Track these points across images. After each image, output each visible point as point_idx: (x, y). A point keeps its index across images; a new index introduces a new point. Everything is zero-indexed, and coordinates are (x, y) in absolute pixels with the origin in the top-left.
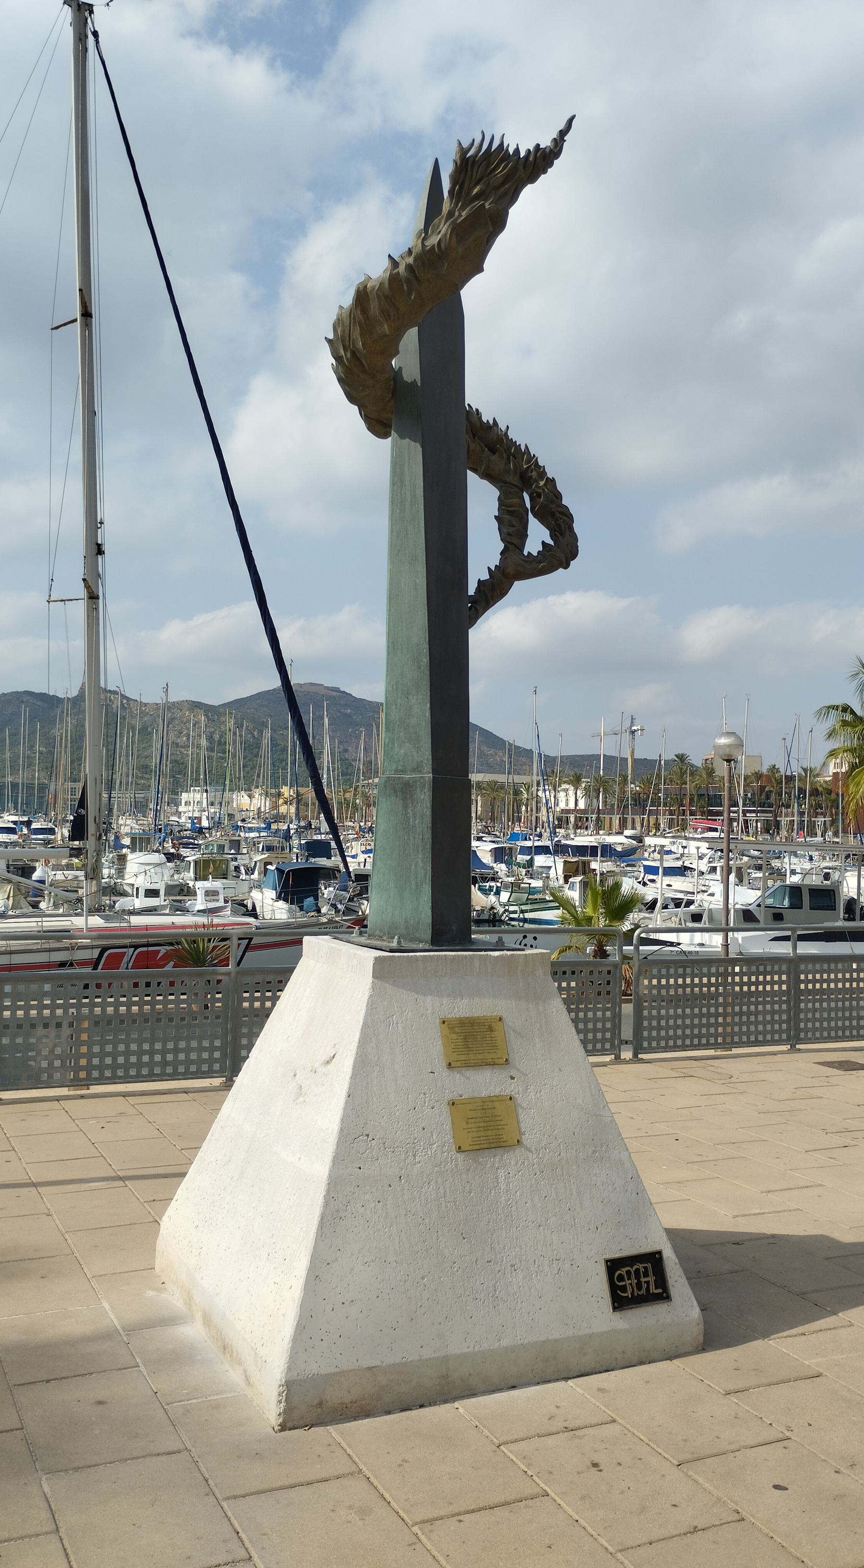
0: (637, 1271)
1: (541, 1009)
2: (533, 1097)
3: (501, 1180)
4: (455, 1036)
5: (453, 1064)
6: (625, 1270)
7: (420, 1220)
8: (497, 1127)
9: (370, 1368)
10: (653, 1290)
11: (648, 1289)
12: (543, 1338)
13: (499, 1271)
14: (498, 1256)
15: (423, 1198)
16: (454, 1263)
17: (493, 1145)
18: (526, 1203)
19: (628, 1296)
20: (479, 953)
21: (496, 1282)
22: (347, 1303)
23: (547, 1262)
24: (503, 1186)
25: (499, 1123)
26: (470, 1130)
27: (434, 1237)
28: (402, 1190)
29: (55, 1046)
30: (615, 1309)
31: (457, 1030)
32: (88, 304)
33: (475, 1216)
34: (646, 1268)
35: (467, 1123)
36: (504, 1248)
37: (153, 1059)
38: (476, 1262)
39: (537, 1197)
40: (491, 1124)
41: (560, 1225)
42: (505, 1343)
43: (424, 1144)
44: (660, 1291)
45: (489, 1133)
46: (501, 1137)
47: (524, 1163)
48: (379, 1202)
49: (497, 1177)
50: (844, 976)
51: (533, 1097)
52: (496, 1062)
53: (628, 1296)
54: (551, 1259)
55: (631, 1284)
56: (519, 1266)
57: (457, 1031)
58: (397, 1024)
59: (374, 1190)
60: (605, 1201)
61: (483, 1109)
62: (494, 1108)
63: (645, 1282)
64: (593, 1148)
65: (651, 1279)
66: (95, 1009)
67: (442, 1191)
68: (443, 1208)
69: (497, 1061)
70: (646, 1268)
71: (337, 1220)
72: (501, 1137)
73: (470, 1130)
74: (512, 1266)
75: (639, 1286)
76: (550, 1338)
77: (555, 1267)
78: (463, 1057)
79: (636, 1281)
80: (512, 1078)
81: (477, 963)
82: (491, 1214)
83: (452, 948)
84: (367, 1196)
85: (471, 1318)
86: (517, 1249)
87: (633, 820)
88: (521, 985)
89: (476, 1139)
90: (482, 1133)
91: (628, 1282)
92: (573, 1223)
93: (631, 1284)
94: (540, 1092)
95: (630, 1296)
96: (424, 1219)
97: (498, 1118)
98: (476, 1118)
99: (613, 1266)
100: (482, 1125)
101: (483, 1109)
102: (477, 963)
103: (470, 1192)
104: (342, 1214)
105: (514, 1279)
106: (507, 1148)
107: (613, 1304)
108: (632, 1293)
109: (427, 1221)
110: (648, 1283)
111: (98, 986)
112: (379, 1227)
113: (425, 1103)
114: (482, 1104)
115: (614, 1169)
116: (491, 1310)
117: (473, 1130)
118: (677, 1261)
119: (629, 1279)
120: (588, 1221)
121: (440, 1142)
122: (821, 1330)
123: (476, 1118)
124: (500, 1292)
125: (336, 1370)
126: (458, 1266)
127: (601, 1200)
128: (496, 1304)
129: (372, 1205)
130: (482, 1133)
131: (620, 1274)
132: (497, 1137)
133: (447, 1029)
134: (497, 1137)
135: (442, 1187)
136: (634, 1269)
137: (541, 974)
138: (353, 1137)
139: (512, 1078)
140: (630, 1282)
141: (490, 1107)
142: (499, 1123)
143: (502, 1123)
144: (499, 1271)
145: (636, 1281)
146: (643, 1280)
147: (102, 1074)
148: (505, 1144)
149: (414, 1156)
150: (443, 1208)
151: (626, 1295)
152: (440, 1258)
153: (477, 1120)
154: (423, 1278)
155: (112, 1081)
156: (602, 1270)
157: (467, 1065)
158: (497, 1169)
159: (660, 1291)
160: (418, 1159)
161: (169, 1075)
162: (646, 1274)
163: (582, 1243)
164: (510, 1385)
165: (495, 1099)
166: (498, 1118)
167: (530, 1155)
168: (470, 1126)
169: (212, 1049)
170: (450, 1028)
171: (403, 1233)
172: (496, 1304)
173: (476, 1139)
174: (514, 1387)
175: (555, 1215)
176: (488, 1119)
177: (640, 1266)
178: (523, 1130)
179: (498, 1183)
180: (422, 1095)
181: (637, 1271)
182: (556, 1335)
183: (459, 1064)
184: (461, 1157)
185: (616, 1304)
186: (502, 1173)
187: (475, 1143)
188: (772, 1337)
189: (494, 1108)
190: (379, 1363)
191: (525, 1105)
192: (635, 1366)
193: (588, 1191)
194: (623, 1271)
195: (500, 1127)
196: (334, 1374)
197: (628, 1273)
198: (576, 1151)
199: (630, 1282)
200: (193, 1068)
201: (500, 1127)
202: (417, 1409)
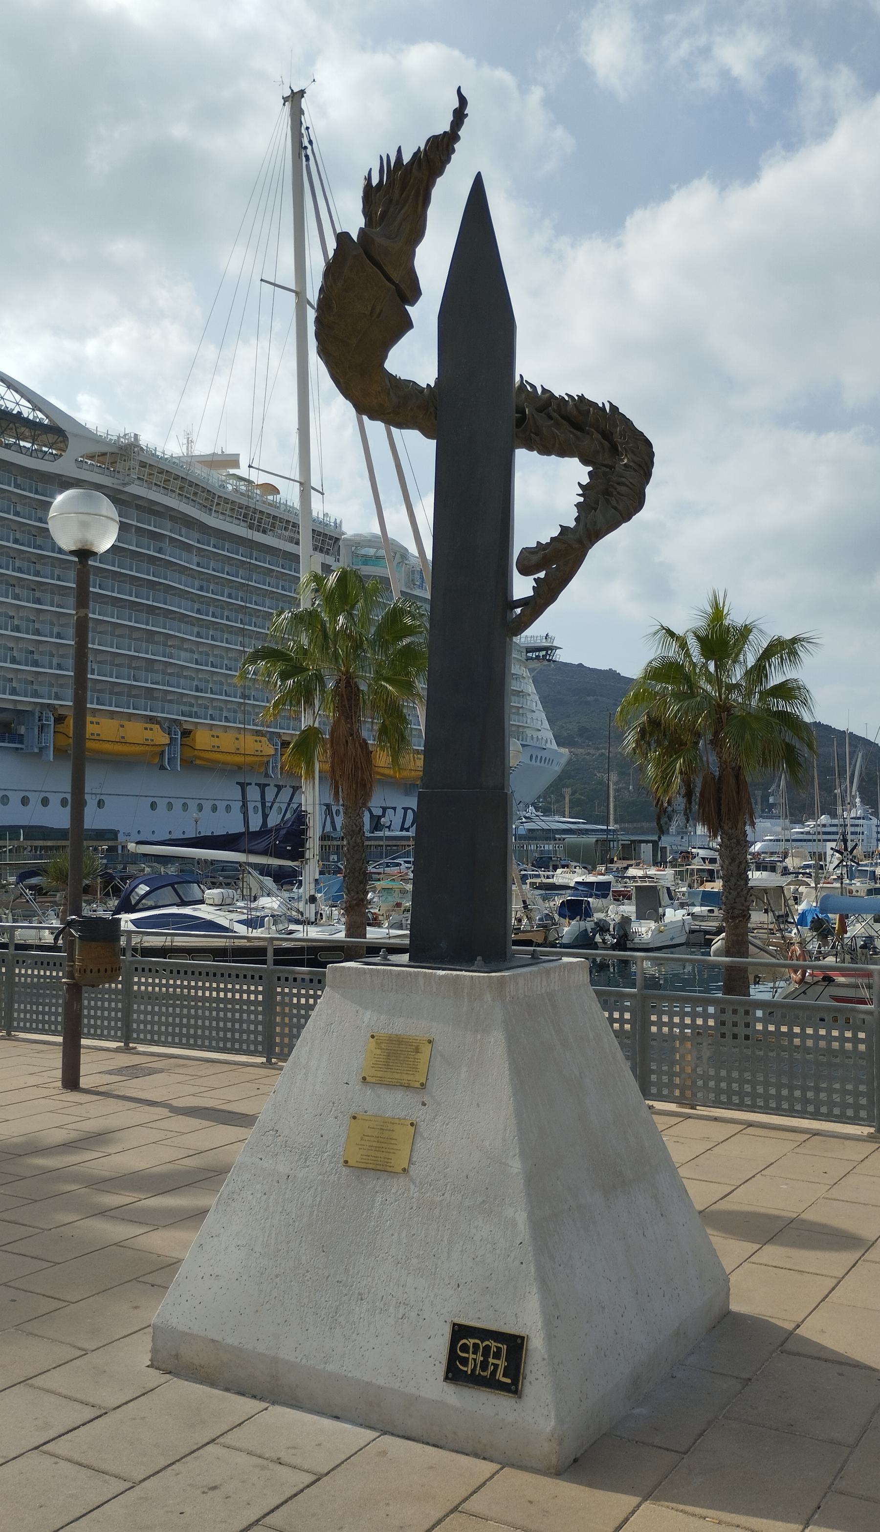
0: (487, 1349)
1: (479, 1037)
2: (438, 1127)
3: (377, 1204)
4: (378, 1052)
5: (368, 1079)
6: (472, 1341)
7: (291, 1222)
8: (389, 1150)
9: (213, 1341)
10: (499, 1375)
11: (494, 1373)
12: (366, 1379)
13: (346, 1295)
14: (349, 1280)
15: (300, 1200)
16: (308, 1272)
17: (378, 1167)
18: (392, 1235)
19: (467, 1371)
20: (424, 970)
21: (340, 1305)
22: (214, 1276)
23: (394, 1303)
24: (376, 1212)
25: (392, 1147)
26: (361, 1147)
27: (298, 1242)
28: (286, 1188)
29: (697, 1066)
30: (446, 1378)
31: (383, 1046)
32: (104, 449)
33: (339, 1233)
34: (499, 1349)
35: (362, 1139)
36: (358, 1273)
37: (793, 1094)
38: (328, 1277)
39: (405, 1232)
40: (384, 1145)
41: (419, 1269)
42: (330, 1368)
43: (317, 1150)
44: (509, 1381)
45: (379, 1154)
46: (389, 1161)
47: (403, 1194)
48: (265, 1194)
49: (374, 1200)
50: (233, 996)
51: (438, 1127)
52: (412, 1085)
53: (467, 1371)
54: (399, 1301)
55: (475, 1360)
56: (366, 1296)
57: (383, 1047)
58: (333, 1032)
59: (265, 1182)
60: (478, 1259)
61: (381, 1129)
62: (393, 1130)
63: (492, 1364)
64: (484, 1198)
65: (502, 1363)
66: (795, 1040)
67: (318, 1200)
68: (314, 1216)
69: (413, 1084)
70: (499, 1349)
71: (230, 1201)
72: (389, 1161)
73: (361, 1147)
74: (360, 1294)
75: (484, 1365)
76: (374, 1381)
77: (401, 1311)
78: (380, 1074)
79: (482, 1359)
80: (424, 1104)
81: (421, 981)
82: (356, 1236)
83: (458, 967)
84: (258, 1186)
85: (307, 1330)
86: (370, 1279)
87: (837, 833)
88: (465, 1008)
89: (364, 1157)
90: (373, 1153)
91: (472, 1356)
92: (433, 1271)
93: (475, 1360)
94: (447, 1124)
95: (469, 1372)
96: (294, 1221)
97: (393, 1142)
98: (372, 1136)
99: (459, 1332)
100: (375, 1144)
101: (381, 1129)
102: (421, 981)
103: (343, 1208)
104: (235, 1196)
105: (357, 1309)
106: (392, 1174)
107: (447, 1372)
108: (473, 1370)
109: (297, 1224)
110: (496, 1366)
111: (287, 979)
112: (257, 1217)
113: (331, 1111)
114: (382, 1124)
115: (502, 1227)
116: (327, 1330)
117: (365, 1147)
118: (546, 1357)
119: (474, 1353)
120: (451, 1274)
121: (331, 1152)
122: (738, 1526)
123: (372, 1136)
124: (340, 1316)
125: (188, 1331)
126: (310, 1276)
127: (473, 1256)
128: (333, 1326)
129: (259, 1195)
130: (373, 1153)
131: (465, 1344)
132: (386, 1160)
133: (374, 1043)
134: (386, 1160)
135: (319, 1196)
136: (484, 1345)
137: (489, 1000)
138: (265, 1130)
139: (424, 1104)
140: (474, 1356)
141: (389, 1128)
142: (392, 1147)
143: (396, 1147)
144: (346, 1295)
145: (482, 1359)
146: (491, 1360)
147: (660, 1091)
148: (390, 1169)
149: (306, 1160)
150: (314, 1216)
151: (465, 1369)
152: (296, 1263)
153: (372, 1139)
154: (277, 1276)
155: (752, 1109)
156: (446, 1332)
157: (382, 1083)
158: (377, 1192)
159: (509, 1381)
160: (308, 1163)
161: (836, 1116)
162: (497, 1356)
163: (436, 1296)
164: (335, 1415)
165: (397, 1121)
166: (393, 1142)
167: (412, 1187)
168: (363, 1142)
169: (857, 1094)
170: (377, 1043)
171: (274, 1229)
172: (333, 1326)
173: (364, 1157)
174: (337, 1418)
175: (418, 1257)
176: (382, 1140)
177: (493, 1345)
178: (414, 1160)
179: (372, 1207)
180: (331, 1104)
181: (487, 1349)
182: (381, 1381)
183: (373, 1080)
184: (345, 1171)
185: (450, 1375)
186: (379, 1198)
187: (363, 1161)
188: (662, 1503)
189: (393, 1130)
190: (220, 1339)
191: (425, 1135)
192: (467, 1454)
193: (461, 1243)
194: (471, 1342)
195: (392, 1151)
196: (186, 1334)
197: (476, 1346)
198: (463, 1195)
199: (474, 1356)
200: (837, 1111)
201: (392, 1151)
202: (248, 1397)
